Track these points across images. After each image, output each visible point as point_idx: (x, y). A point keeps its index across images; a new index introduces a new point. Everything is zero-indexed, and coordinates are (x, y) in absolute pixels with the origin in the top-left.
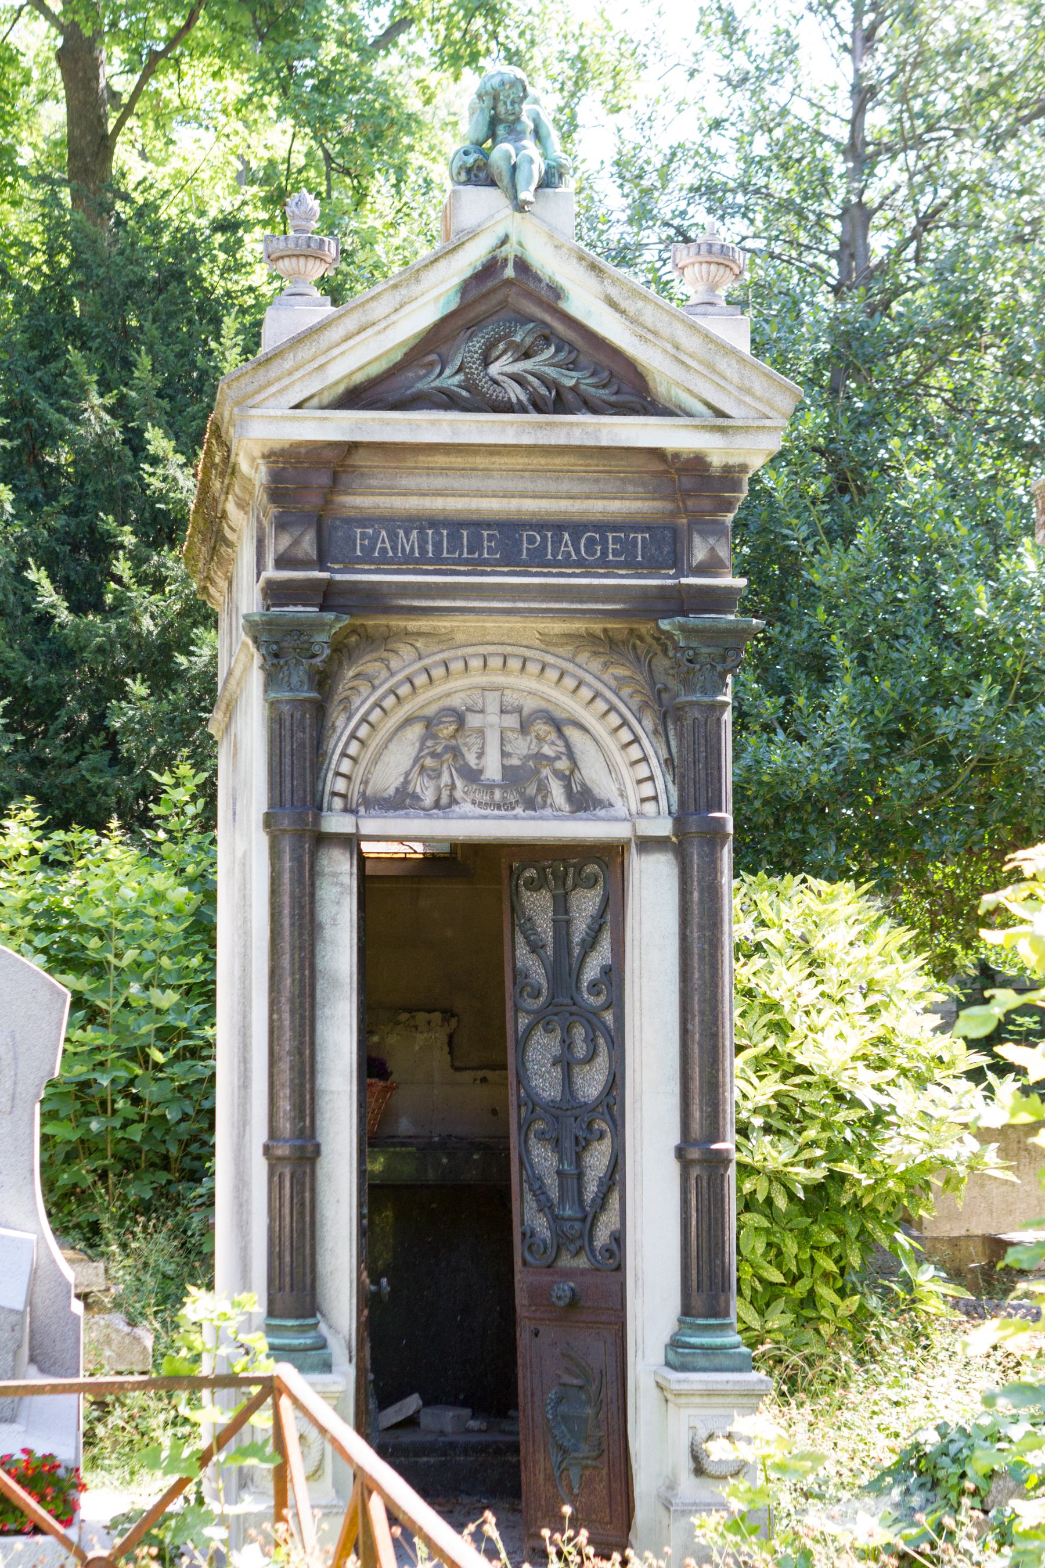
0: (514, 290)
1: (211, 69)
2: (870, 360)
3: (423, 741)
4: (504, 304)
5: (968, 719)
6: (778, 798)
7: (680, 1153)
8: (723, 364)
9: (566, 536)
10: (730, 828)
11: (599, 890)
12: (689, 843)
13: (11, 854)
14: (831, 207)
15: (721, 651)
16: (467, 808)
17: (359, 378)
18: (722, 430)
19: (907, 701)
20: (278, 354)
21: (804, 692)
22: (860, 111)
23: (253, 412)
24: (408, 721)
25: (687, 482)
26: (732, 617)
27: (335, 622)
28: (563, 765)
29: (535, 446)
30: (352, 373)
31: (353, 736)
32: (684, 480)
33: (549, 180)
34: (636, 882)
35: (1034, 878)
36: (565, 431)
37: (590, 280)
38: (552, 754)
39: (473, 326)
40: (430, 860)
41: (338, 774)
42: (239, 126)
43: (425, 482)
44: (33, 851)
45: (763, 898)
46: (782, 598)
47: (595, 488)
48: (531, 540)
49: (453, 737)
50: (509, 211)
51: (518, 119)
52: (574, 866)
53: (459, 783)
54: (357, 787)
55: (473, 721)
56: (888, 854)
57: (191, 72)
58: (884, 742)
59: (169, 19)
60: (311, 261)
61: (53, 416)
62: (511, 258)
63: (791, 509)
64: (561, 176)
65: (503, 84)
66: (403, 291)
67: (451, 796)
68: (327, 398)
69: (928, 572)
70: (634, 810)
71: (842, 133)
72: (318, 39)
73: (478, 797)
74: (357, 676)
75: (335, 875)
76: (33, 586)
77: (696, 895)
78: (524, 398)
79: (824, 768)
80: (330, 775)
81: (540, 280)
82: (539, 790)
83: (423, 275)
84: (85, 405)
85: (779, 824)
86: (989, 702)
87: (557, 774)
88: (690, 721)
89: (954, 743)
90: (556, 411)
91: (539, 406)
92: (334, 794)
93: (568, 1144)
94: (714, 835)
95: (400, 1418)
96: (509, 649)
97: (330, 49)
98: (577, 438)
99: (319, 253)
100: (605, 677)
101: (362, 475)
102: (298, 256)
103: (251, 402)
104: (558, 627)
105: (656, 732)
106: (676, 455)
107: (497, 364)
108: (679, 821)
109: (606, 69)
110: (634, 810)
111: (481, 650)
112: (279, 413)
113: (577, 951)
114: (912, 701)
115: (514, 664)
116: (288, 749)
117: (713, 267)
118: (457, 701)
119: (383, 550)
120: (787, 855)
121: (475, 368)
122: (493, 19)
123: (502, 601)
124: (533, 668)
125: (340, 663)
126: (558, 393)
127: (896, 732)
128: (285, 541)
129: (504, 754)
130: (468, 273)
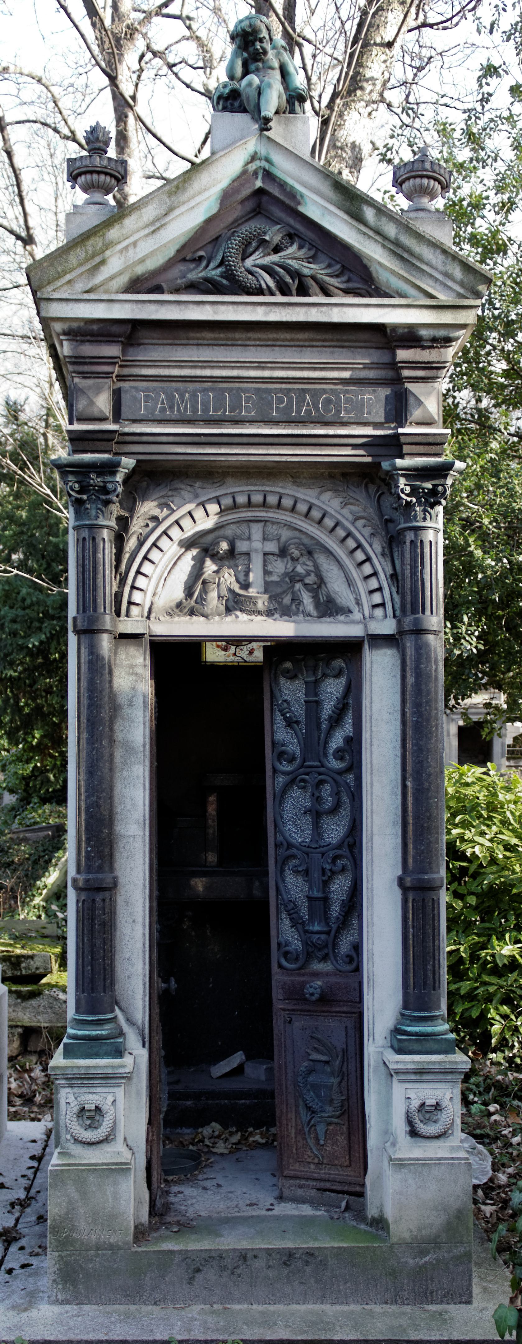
7: (401, 881)
11: (343, 680)
28: (310, 580)
34: (368, 672)
91: (284, 290)
93: (316, 875)
95: (228, 1070)
98: (314, 315)
105: (383, 554)
113: (324, 726)
129: (266, 573)
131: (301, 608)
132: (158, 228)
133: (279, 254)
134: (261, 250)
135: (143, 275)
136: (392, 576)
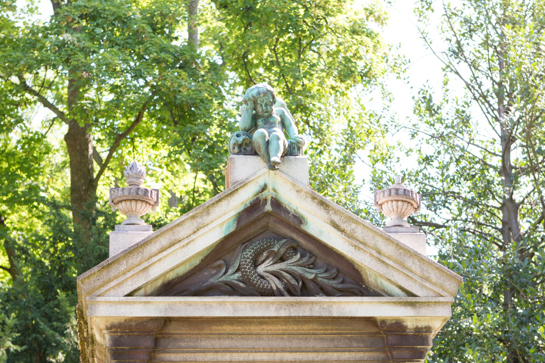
0: (272, 219)
1: (152, 144)
8: (409, 263)
14: (494, 203)
17: (171, 276)
22: (506, 150)
23: (99, 299)
25: (392, 339)
29: (290, 317)
32: (390, 338)
33: (292, 150)
39: (247, 242)
42: (169, 174)
43: (217, 343)
47: (331, 345)
50: (266, 170)
51: (271, 115)
57: (141, 145)
59: (127, 118)
60: (139, 204)
62: (269, 199)
64: (299, 149)
65: (259, 93)
66: (199, 220)
68: (149, 289)
71: (497, 162)
72: (208, 124)
78: (281, 286)
81: (288, 212)
83: (212, 210)
84: (68, 325)
90: (302, 295)
97: (213, 131)
98: (317, 312)
101: (175, 339)
102: (130, 200)
103: (98, 292)
106: (383, 322)
112: (117, 299)
117: (400, 203)
121: (248, 268)
122: (306, 113)
126: (303, 284)
130: (241, 208)
132: (189, 243)
133: (286, 262)
134: (271, 259)
135: (173, 279)
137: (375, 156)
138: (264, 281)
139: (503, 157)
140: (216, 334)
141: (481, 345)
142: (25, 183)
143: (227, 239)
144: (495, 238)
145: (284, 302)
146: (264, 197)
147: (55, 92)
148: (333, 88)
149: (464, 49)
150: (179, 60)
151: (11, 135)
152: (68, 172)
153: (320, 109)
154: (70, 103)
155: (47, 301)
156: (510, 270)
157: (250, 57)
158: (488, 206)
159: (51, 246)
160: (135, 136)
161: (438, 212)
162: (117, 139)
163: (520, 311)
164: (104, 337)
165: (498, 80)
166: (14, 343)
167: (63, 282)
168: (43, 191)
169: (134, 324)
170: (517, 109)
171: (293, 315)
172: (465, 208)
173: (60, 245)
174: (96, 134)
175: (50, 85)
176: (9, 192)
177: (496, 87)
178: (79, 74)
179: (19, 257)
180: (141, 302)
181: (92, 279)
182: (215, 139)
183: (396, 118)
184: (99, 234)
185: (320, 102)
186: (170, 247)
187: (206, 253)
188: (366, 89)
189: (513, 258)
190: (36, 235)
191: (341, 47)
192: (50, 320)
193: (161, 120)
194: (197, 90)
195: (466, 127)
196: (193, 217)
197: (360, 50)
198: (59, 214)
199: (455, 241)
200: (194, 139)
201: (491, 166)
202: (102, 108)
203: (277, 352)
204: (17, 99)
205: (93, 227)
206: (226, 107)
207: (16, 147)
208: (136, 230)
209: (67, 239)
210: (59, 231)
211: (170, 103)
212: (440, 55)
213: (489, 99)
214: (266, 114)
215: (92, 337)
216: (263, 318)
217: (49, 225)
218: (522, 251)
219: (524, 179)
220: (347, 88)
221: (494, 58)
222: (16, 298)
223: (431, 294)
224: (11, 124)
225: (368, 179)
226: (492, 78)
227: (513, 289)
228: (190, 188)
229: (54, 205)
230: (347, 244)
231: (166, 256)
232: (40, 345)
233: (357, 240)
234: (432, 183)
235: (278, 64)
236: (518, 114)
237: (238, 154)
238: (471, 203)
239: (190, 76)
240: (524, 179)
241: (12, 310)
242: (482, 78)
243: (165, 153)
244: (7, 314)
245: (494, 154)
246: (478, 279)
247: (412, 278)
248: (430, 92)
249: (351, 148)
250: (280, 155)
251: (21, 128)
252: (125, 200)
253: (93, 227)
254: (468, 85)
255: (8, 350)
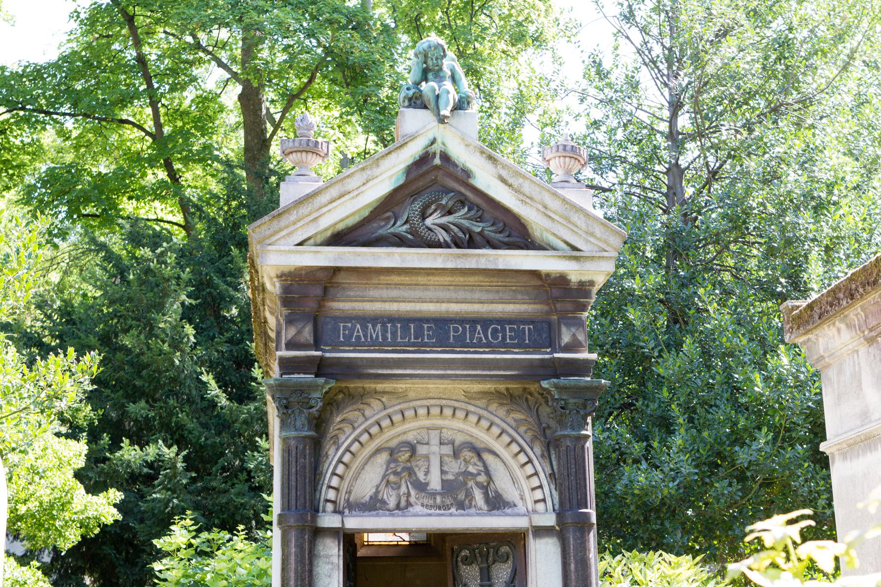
0: (441, 172)
2: (686, 249)
3: (388, 463)
4: (434, 182)
5: (755, 454)
6: (645, 504)
8: (575, 218)
9: (479, 327)
10: (594, 519)
12: (568, 530)
13: (174, 547)
15: (583, 401)
16: (418, 509)
17: (341, 227)
18: (577, 259)
19: (719, 444)
20: (287, 210)
21: (657, 439)
23: (270, 248)
24: (378, 451)
25: (556, 292)
26: (589, 379)
27: (325, 384)
28: (482, 478)
30: (336, 224)
31: (340, 461)
32: (553, 290)
33: (461, 105)
35: (772, 548)
36: (475, 259)
37: (489, 166)
38: (475, 472)
39: (416, 195)
40: (414, 546)
41: (330, 487)
43: (385, 293)
44: (190, 545)
45: (636, 566)
46: (644, 385)
47: (496, 296)
48: (456, 330)
49: (409, 461)
51: (441, 69)
52: (493, 547)
53: (413, 492)
54: (343, 496)
55: (422, 450)
56: (715, 538)
58: (706, 469)
59: (300, 78)
60: (310, 155)
61: (223, 287)
63: (644, 331)
64: (468, 103)
65: (430, 47)
66: (369, 172)
67: (407, 501)
68: (319, 239)
69: (727, 368)
70: (530, 508)
71: (664, 127)
72: (380, 86)
73: (425, 502)
74: (342, 421)
75: (328, 556)
76: (205, 384)
77: (573, 566)
78: (448, 239)
79: (671, 485)
80: (324, 488)
81: (457, 166)
82: (466, 496)
85: (647, 520)
86: (767, 443)
87: (478, 485)
88: (564, 448)
89: (747, 468)
92: (327, 501)
94: (583, 525)
96: (444, 402)
97: (385, 92)
98: (483, 264)
99: (315, 150)
100: (509, 420)
101: (344, 288)
102: (301, 152)
103: (268, 242)
104: (476, 387)
105: (543, 456)
106: (548, 275)
107: (431, 218)
108: (560, 516)
109: (532, 94)
110: (530, 508)
111: (426, 402)
112: (287, 248)
114: (722, 443)
115: (448, 412)
116: (294, 470)
117: (567, 159)
118: (410, 437)
119: (358, 337)
120: (652, 540)
121: (416, 220)
122: (476, 76)
123: (437, 369)
124: (460, 414)
125: (332, 413)
126: (470, 236)
127: (713, 462)
128: (292, 331)
129: (443, 472)
130: (410, 161)
131: (473, 503)
135: (343, 230)
136: (550, 475)
137: (544, 121)
138: (432, 234)
139: (670, 122)
140: (383, 284)
141: (642, 304)
142: (200, 142)
143: (396, 191)
144: (659, 203)
145: (451, 254)
146: (433, 150)
147: (229, 53)
148: (504, 52)
149: (636, 13)
150: (352, 21)
151: (185, 94)
152: (241, 133)
153: (491, 73)
154: (243, 63)
155: (221, 257)
156: (674, 233)
157: (422, 20)
158: (654, 171)
159: (225, 204)
160: (308, 97)
161: (604, 176)
162: (291, 99)
163: (682, 273)
164: (274, 286)
165: (668, 45)
166: (189, 296)
167: (237, 238)
168: (217, 149)
169: (303, 272)
170: (685, 75)
171: (459, 267)
172: (631, 173)
173: (234, 203)
174: (269, 94)
175: (224, 45)
176: (183, 150)
177: (666, 52)
178: (252, 33)
179: (194, 214)
180: (310, 252)
181: (263, 228)
182: (386, 101)
183: (566, 82)
184: (272, 192)
185: (491, 65)
186: (340, 198)
187: (375, 205)
188: (536, 52)
189: (677, 222)
190: (210, 192)
191: (513, 11)
192: (224, 276)
193: (334, 81)
194: (369, 51)
195: (635, 92)
196: (363, 169)
197: (532, 14)
198: (233, 173)
199: (620, 204)
200: (365, 101)
201: (658, 132)
202: (276, 68)
203: (443, 302)
204: (191, 57)
205: (267, 186)
206: (399, 70)
207: (190, 106)
208: (307, 181)
209: (240, 197)
210: (233, 189)
211: (342, 64)
212: (611, 19)
213: (659, 64)
214: (437, 68)
215: (263, 285)
216: (431, 269)
217: (223, 183)
218: (685, 215)
219: (690, 145)
220: (518, 53)
221: (666, 24)
222: (191, 254)
223: (596, 249)
224: (186, 83)
225: (537, 141)
226: (662, 43)
227: (674, 252)
228: (361, 149)
229: (228, 164)
230: (514, 198)
231: (335, 208)
232: (214, 299)
233: (524, 195)
234: (599, 147)
235: (450, 26)
236: (687, 80)
237: (408, 107)
238: (637, 168)
239: (362, 38)
240: (690, 145)
241: (188, 265)
242: (653, 44)
243: (337, 114)
244: (182, 269)
245: (662, 119)
246: (641, 241)
247: (577, 233)
248: (600, 56)
249: (520, 110)
250: (450, 108)
251: (195, 87)
252: (296, 152)
253: (267, 186)
254: (638, 51)
255: (183, 304)
